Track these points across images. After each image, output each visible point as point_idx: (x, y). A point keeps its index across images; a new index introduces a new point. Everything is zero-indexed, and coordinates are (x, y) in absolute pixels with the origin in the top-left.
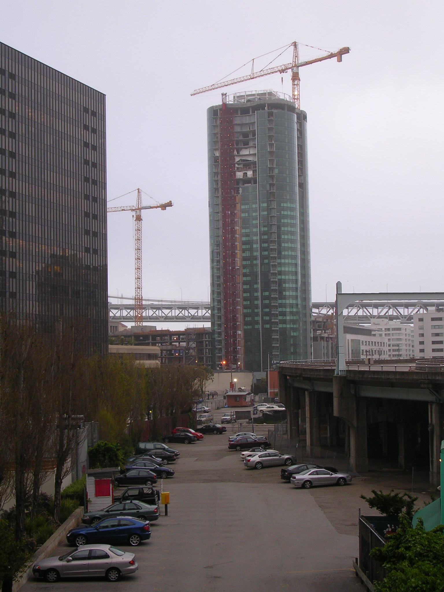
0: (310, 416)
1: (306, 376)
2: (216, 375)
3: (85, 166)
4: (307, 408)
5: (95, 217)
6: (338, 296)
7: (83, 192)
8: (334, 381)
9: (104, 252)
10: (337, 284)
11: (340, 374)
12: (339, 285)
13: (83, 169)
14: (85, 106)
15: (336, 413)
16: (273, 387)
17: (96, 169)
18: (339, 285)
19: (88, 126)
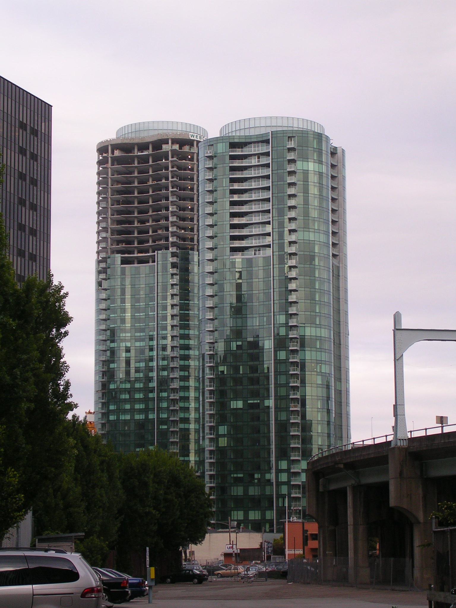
0: (354, 522)
1: (349, 461)
2: (207, 535)
3: (20, 181)
4: (350, 511)
5: (33, 232)
6: (396, 332)
7: (15, 245)
8: (390, 461)
9: (46, 235)
10: (395, 315)
11: (399, 444)
12: (397, 318)
13: (16, 213)
14: (21, 120)
15: (392, 503)
16: (294, 546)
17: (34, 263)
18: (397, 318)
19: (26, 125)
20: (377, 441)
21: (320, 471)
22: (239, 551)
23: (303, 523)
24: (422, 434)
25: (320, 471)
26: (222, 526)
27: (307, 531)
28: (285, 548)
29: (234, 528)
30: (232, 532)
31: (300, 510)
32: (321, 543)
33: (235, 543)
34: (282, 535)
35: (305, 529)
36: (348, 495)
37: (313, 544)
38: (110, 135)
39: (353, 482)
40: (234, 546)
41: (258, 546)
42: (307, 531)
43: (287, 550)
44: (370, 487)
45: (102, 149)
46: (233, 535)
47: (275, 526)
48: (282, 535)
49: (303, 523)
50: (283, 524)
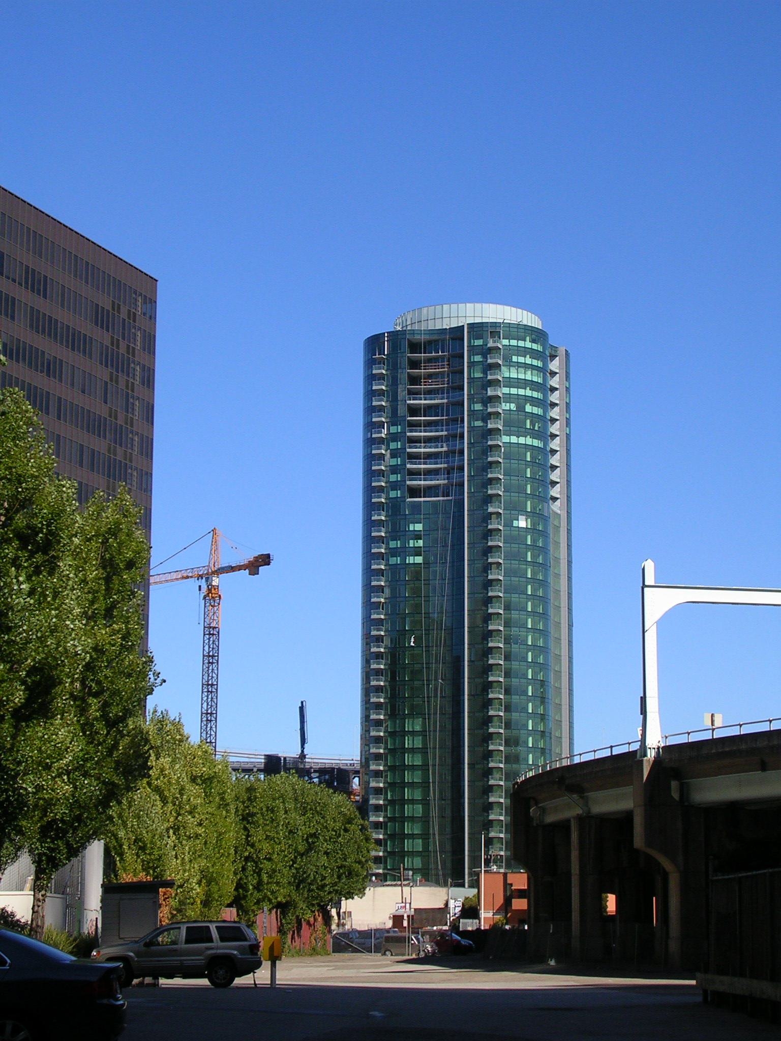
4: (575, 854)
20: (616, 751)
21: (523, 796)
22: (413, 913)
23: (505, 875)
24: (606, 753)
25: (523, 796)
26: (392, 875)
27: (511, 885)
28: (480, 909)
29: (408, 879)
30: (405, 885)
31: (502, 856)
32: (532, 902)
33: (408, 901)
34: (475, 891)
35: (509, 882)
36: (573, 828)
37: (520, 904)
38: (385, 326)
39: (580, 811)
40: (408, 905)
41: (442, 906)
42: (511, 885)
43: (482, 911)
44: (604, 820)
45: (374, 343)
46: (406, 890)
47: (466, 877)
48: (476, 890)
49: (505, 875)
50: (478, 874)
